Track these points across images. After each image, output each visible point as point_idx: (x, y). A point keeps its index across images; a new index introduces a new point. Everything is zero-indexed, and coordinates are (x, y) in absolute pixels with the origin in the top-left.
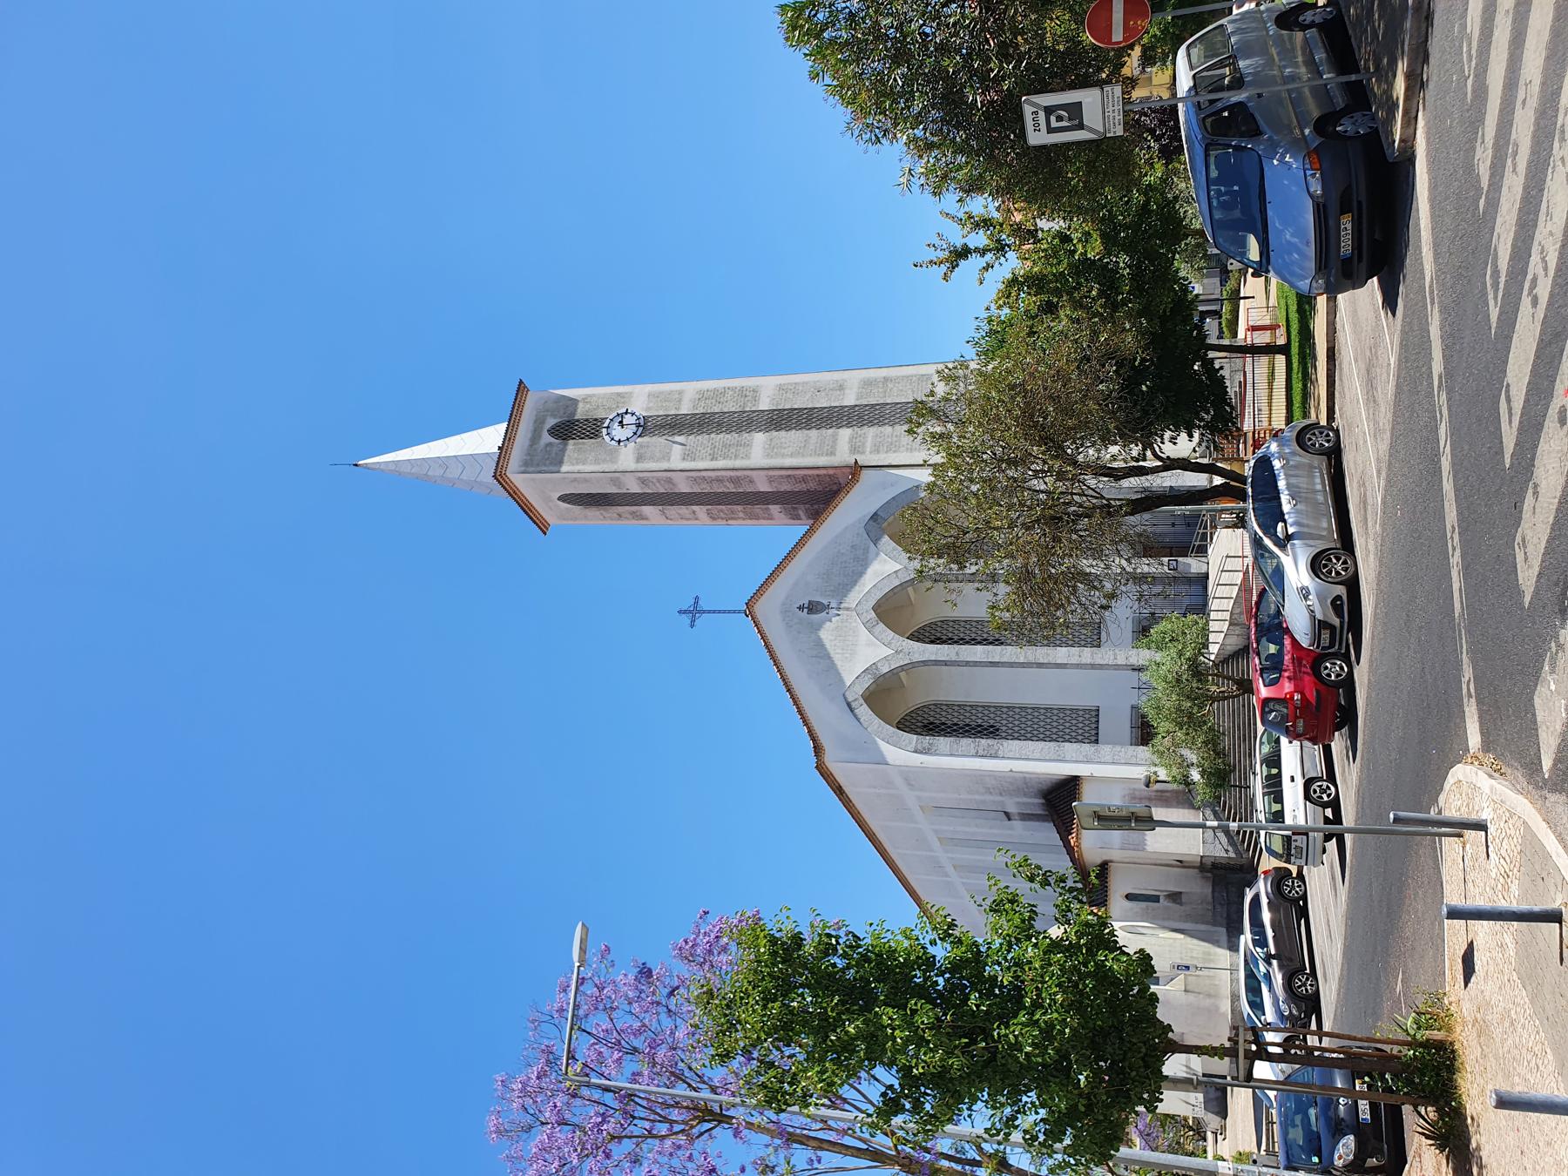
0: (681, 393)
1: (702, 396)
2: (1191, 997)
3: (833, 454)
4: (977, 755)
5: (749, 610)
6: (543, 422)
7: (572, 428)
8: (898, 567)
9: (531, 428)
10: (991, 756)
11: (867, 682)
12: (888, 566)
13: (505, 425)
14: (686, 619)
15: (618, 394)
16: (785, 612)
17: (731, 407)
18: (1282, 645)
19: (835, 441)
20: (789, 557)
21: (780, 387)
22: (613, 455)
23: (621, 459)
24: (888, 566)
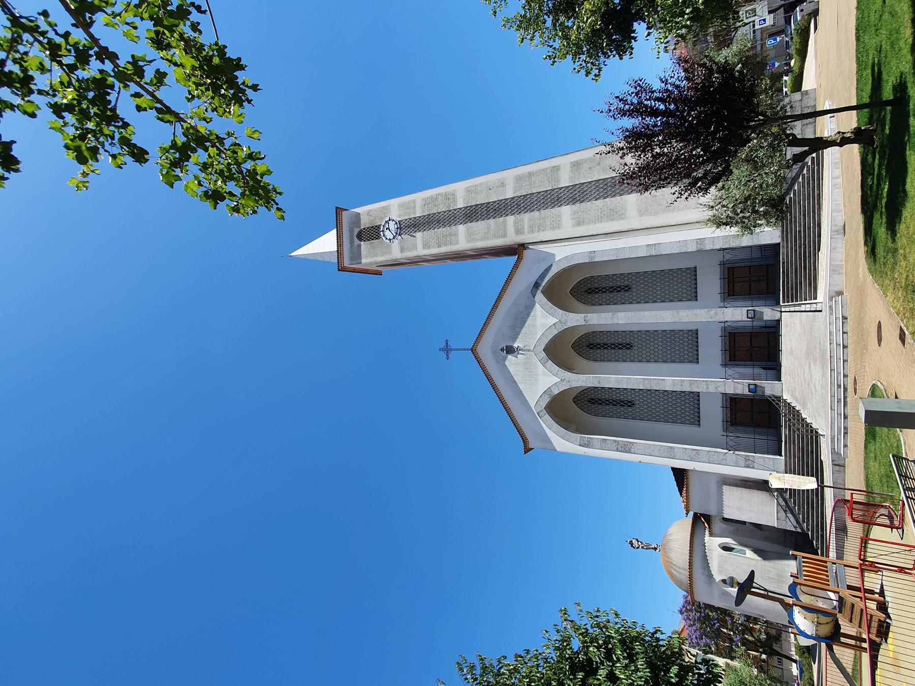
0: (414, 201)
3: (505, 236)
4: (617, 450)
5: (473, 350)
7: (372, 233)
10: (626, 452)
11: (547, 400)
12: (545, 320)
14: (443, 345)
15: (384, 208)
16: (494, 352)
17: (442, 208)
20: (499, 298)
21: (519, 179)
23: (394, 249)
24: (545, 320)
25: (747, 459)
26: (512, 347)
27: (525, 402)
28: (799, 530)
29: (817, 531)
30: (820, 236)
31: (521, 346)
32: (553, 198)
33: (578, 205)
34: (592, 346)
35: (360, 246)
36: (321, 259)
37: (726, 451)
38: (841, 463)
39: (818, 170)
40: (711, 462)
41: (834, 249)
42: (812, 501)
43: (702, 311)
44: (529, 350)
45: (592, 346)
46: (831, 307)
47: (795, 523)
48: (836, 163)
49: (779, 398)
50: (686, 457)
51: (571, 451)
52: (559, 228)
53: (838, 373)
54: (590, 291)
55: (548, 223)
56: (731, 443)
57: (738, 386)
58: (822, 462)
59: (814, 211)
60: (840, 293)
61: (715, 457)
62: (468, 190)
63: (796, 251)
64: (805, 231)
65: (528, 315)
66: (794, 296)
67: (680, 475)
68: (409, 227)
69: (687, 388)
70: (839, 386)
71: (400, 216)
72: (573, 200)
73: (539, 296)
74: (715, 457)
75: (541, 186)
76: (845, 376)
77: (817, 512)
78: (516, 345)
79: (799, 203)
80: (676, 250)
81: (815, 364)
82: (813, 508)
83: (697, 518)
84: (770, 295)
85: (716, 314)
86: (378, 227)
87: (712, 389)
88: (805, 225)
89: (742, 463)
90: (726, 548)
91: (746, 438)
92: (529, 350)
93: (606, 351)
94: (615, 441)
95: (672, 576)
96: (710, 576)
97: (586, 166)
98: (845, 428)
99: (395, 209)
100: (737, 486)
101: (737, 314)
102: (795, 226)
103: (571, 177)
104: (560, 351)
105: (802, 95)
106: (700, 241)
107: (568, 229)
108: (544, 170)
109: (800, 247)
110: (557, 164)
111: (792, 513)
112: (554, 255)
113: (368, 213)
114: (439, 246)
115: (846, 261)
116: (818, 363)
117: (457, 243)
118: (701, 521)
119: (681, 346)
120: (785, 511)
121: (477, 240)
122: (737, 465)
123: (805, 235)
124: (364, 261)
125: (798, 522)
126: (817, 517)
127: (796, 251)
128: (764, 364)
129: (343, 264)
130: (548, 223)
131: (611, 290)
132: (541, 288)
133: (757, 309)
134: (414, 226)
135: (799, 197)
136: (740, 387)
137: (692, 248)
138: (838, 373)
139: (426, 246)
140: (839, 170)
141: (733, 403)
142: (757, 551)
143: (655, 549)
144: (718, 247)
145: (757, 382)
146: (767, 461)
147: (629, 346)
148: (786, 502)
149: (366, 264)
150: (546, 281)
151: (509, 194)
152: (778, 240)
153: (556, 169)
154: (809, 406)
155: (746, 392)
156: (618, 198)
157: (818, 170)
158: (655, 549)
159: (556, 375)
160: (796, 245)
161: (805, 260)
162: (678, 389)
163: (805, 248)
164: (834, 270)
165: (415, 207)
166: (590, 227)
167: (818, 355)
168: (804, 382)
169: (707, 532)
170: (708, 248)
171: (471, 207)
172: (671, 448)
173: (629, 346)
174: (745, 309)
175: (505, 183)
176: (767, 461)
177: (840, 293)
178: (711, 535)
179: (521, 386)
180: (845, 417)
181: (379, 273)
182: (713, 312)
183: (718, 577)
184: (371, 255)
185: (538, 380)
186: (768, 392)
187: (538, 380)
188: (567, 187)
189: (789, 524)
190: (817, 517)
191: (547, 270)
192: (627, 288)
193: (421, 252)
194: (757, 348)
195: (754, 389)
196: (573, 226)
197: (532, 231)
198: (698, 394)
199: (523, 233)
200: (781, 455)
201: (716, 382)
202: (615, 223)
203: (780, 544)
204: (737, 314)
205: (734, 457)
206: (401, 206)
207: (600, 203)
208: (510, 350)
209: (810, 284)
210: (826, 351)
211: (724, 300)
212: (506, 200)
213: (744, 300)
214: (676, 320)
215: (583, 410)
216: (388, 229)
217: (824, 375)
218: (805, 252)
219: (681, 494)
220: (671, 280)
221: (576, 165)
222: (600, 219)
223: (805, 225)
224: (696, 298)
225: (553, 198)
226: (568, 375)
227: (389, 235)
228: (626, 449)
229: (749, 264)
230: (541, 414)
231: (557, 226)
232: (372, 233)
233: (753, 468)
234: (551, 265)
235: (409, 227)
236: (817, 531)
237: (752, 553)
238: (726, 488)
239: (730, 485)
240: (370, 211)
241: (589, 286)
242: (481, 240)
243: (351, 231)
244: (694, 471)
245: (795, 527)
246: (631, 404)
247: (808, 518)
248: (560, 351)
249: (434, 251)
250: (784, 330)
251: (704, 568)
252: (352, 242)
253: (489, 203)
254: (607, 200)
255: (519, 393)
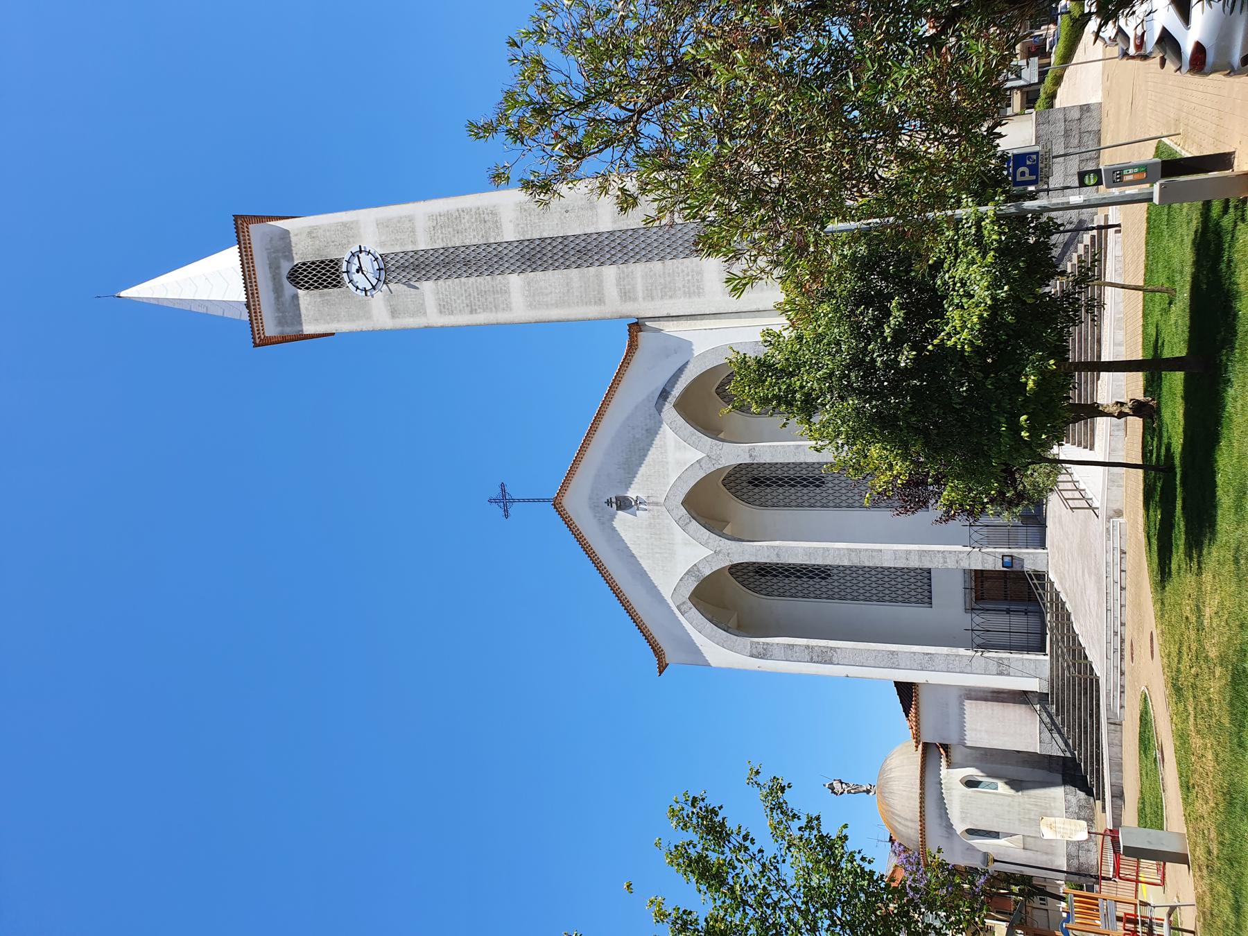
0: (411, 219)
1: (438, 223)
2: (1029, 853)
4: (812, 661)
5: (557, 504)
6: (278, 267)
7: (323, 275)
8: (700, 455)
9: (270, 285)
10: (825, 663)
14: (496, 492)
15: (344, 225)
16: (594, 507)
17: (472, 238)
18: (1012, 89)
19: (600, 284)
24: (680, 456)
26: (626, 498)
28: (1068, 755)
29: (1092, 763)
31: (643, 496)
35: (296, 297)
36: (202, 310)
38: (1118, 721)
40: (947, 669)
42: (1086, 723)
44: (657, 504)
47: (1063, 747)
48: (1119, 320)
50: (915, 666)
51: (736, 666)
52: (699, 294)
55: (679, 285)
56: (979, 641)
57: (990, 559)
60: (1119, 513)
61: (956, 663)
65: (650, 444)
67: (907, 692)
69: (914, 563)
73: (669, 411)
74: (956, 663)
78: (632, 494)
82: (1086, 733)
83: (926, 745)
87: (951, 564)
89: (994, 668)
90: (971, 783)
92: (657, 504)
94: (807, 647)
98: (1122, 686)
104: (706, 504)
111: (1059, 732)
112: (690, 344)
113: (309, 234)
118: (933, 752)
120: (1050, 731)
125: (1067, 744)
129: (265, 333)
130: (679, 285)
132: (672, 399)
134: (416, 267)
136: (991, 559)
140: (1122, 333)
143: (868, 792)
145: (1014, 551)
146: (1027, 664)
148: (1052, 719)
155: (999, 567)
158: (868, 792)
159: (705, 545)
165: (413, 231)
171: (531, 241)
172: (893, 653)
176: (1027, 664)
178: (949, 766)
179: (645, 564)
180: (1122, 673)
183: (959, 828)
185: (672, 554)
186: (1028, 566)
187: (672, 554)
189: (1056, 748)
190: (1092, 745)
191: (681, 370)
195: (1010, 561)
197: (650, 296)
198: (929, 571)
199: (635, 300)
203: (1043, 769)
205: (983, 661)
206: (382, 224)
208: (623, 504)
212: (599, 234)
216: (359, 270)
219: (907, 716)
226: (725, 543)
228: (825, 658)
230: (683, 608)
232: (323, 275)
233: (1008, 675)
236: (1092, 763)
237: (1007, 787)
238: (967, 702)
242: (556, 305)
243: (274, 267)
244: (927, 684)
245: (1063, 751)
247: (1080, 745)
251: (941, 817)
252: (278, 290)
253: (565, 238)
255: (641, 575)
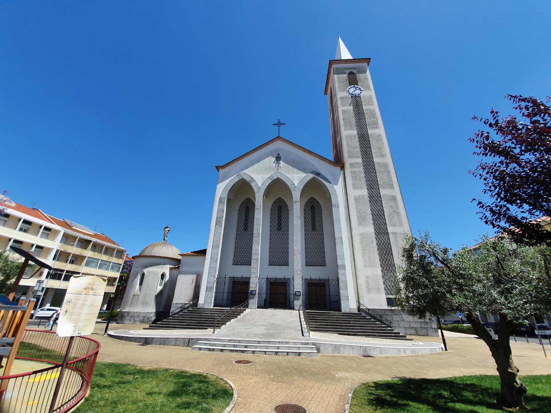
0: (373, 104)
2: (132, 297)
3: (349, 157)
4: (217, 218)
5: (278, 138)
7: (353, 80)
8: (296, 185)
10: (216, 223)
11: (247, 179)
12: (296, 179)
13: (351, 58)
15: (369, 87)
17: (368, 121)
20: (310, 153)
21: (386, 165)
22: (344, 90)
23: (342, 92)
24: (296, 179)
25: (212, 288)
26: (280, 160)
27: (247, 167)
28: (171, 314)
30: (348, 335)
31: (281, 165)
32: (373, 185)
33: (368, 199)
34: (280, 209)
35: (345, 73)
37: (216, 277)
39: (392, 336)
40: (210, 270)
41: (352, 348)
43: (300, 267)
44: (278, 169)
45: (280, 209)
46: (307, 344)
47: (175, 312)
49: (247, 306)
51: (217, 192)
53: (256, 347)
54: (313, 208)
56: (221, 280)
57: (254, 285)
58: (206, 329)
59: (364, 332)
60: (318, 350)
62: (379, 136)
63: (337, 320)
64: (351, 326)
65: (300, 170)
66: (309, 319)
67: (203, 252)
68: (356, 102)
69: (254, 257)
70: (246, 347)
71: (364, 96)
72: (371, 197)
75: (381, 178)
76: (253, 352)
77: (177, 325)
78: (281, 162)
79: (368, 324)
80: (338, 253)
81: (265, 329)
82: (180, 322)
83: (179, 261)
84: (309, 305)
85: (298, 274)
86: (357, 84)
87: (253, 270)
88: (354, 326)
89: (209, 285)
90: (163, 276)
91: (226, 287)
92: (278, 169)
93: (277, 216)
94: (223, 217)
95: (148, 247)
96: (147, 267)
97: (393, 204)
98: (213, 350)
99: (368, 93)
100: (196, 282)
101: (298, 286)
102: (353, 321)
103: (386, 195)
104: (277, 187)
105: (436, 329)
106: (344, 267)
107: (352, 193)
108: (391, 180)
109: (340, 323)
110: (395, 188)
114: (344, 119)
115: (344, 357)
116: (266, 331)
117: (345, 130)
118: (176, 263)
119: (279, 255)
120: (181, 307)
121: (347, 141)
122: (208, 282)
123: (348, 326)
124: (336, 76)
126: (174, 325)
127: (337, 320)
128: (268, 300)
131: (313, 220)
133: (301, 297)
135: (372, 324)
136: (254, 286)
137: (339, 262)
138: (256, 347)
139: (344, 112)
141: (246, 282)
142: (161, 292)
143: (164, 240)
144: (340, 276)
145: (257, 295)
147: (279, 229)
149: (333, 78)
150: (321, 179)
151: (376, 160)
152: (343, 310)
153: (391, 187)
154: (238, 324)
155: (251, 289)
156: (372, 222)
157: (392, 336)
158: (164, 240)
159: (263, 184)
160: (341, 320)
161: (332, 325)
162: (253, 252)
163: (339, 326)
164: (336, 348)
165: (369, 105)
166: (354, 206)
167: (271, 331)
168: (255, 322)
169: (172, 266)
170: (339, 271)
172: (219, 247)
173: (279, 229)
174: (301, 290)
175: (383, 157)
177: (318, 350)
178: (171, 269)
179: (256, 165)
181: (326, 93)
182: (299, 272)
183: (146, 271)
184: (338, 81)
186: (251, 301)
188: (380, 193)
189: (174, 309)
190: (174, 325)
192: (314, 229)
193: (341, 109)
194: (277, 296)
195: (253, 294)
196: (355, 196)
198: (250, 265)
199: (351, 167)
200: (214, 306)
201: (257, 274)
202: (356, 220)
204: (298, 286)
206: (370, 97)
207: (369, 212)
208: (278, 159)
209: (316, 327)
210: (274, 338)
211: (306, 280)
212: (372, 158)
213: (306, 291)
214: (295, 252)
215: (241, 200)
217: (256, 335)
218: (337, 326)
220: (319, 249)
221: (394, 199)
222: (359, 211)
223: (354, 326)
224: (307, 265)
225: (373, 185)
227: (351, 91)
228: (218, 223)
229: (327, 294)
230: (239, 176)
231: (355, 187)
232: (353, 80)
233: (206, 291)
234: (330, 183)
235: (356, 102)
238: (194, 277)
239: (197, 279)
240: (367, 79)
241: (317, 207)
242: (347, 144)
243: (355, 68)
244: (205, 259)
245: (172, 312)
246: (246, 229)
248: (277, 187)
249: (341, 117)
250: (287, 312)
251: (151, 263)
252: (348, 69)
254: (371, 216)
255: (252, 164)
